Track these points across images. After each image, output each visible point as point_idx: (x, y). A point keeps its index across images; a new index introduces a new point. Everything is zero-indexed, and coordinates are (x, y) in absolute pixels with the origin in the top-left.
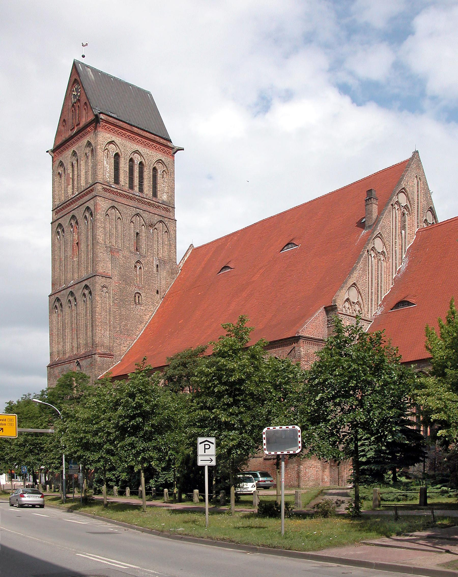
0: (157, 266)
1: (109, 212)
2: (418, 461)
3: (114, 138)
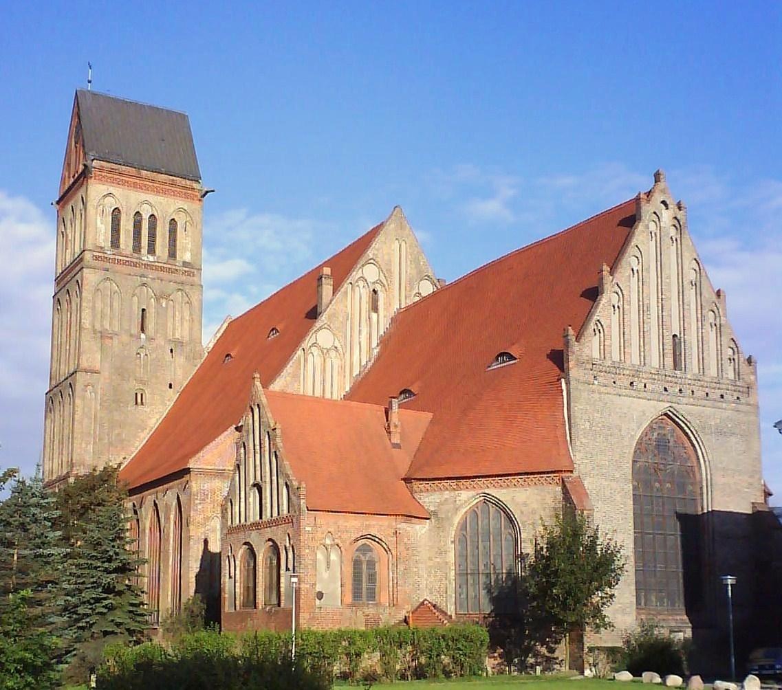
0: (172, 351)
1: (101, 286)
2: (139, 664)
3: (112, 190)
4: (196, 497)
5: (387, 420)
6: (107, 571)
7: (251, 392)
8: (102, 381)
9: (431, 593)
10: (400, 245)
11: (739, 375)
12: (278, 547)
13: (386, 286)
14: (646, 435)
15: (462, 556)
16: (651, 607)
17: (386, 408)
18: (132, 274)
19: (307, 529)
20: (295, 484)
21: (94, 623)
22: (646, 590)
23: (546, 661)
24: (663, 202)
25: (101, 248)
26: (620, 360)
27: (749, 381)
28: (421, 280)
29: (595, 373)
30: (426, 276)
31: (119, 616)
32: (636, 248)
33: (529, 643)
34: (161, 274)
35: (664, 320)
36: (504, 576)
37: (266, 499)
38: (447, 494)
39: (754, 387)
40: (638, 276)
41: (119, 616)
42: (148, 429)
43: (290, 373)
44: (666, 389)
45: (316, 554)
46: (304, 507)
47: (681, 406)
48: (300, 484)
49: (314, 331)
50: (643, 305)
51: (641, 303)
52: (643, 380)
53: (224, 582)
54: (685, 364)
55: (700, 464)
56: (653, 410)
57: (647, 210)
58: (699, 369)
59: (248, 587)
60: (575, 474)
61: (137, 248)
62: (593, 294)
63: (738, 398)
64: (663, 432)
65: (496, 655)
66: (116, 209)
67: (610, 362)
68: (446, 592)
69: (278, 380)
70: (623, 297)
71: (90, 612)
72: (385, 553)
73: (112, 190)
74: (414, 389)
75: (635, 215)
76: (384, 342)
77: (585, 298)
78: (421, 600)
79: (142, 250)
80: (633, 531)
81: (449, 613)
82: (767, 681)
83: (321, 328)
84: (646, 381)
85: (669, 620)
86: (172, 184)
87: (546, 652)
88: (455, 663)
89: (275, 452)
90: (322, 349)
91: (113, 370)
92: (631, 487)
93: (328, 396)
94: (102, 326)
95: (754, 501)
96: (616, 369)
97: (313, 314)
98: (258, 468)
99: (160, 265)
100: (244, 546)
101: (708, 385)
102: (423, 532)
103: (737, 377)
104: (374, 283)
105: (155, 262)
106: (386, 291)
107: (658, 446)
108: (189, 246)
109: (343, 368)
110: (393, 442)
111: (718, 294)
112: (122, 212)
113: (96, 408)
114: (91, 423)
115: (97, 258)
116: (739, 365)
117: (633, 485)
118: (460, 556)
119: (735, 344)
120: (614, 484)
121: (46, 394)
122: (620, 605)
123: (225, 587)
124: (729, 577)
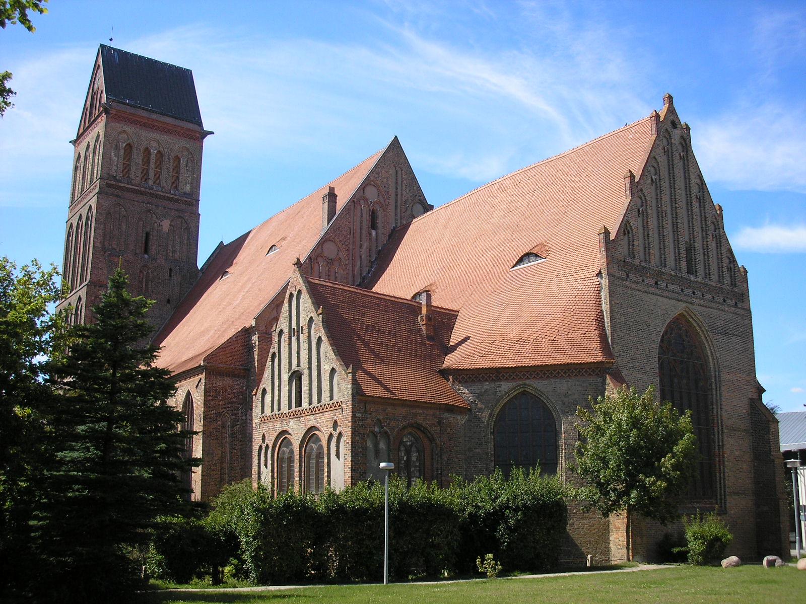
47: (695, 307)
67: (639, 261)
73: (125, 128)
95: (750, 397)
120: (645, 377)
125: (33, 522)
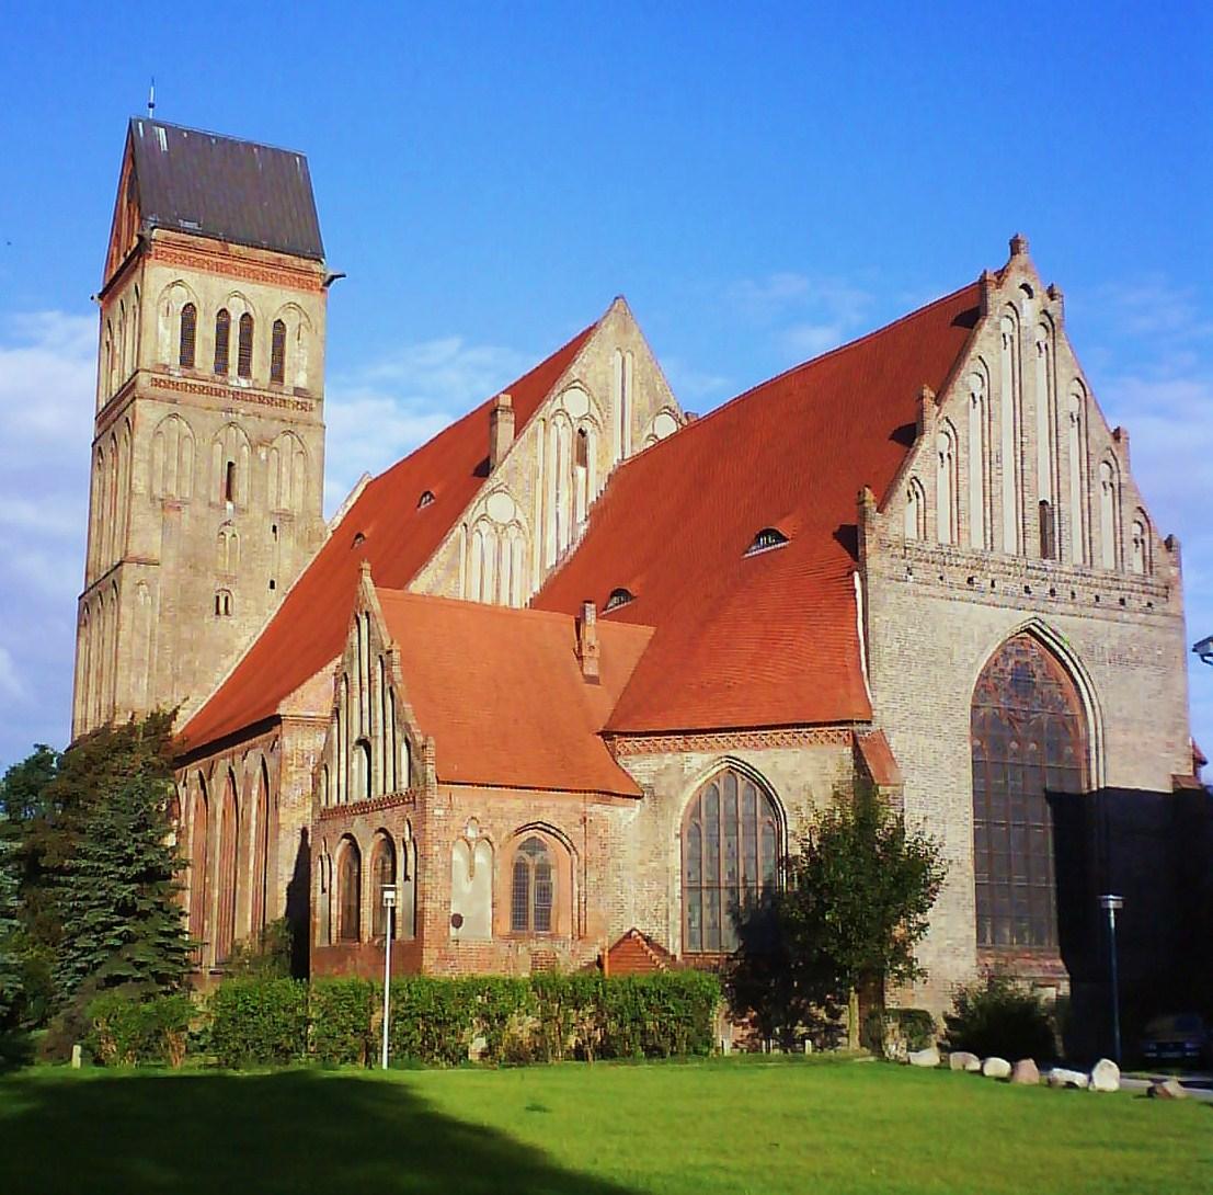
0: (274, 529)
1: (163, 428)
4: (290, 762)
5: (579, 639)
6: (123, 879)
7: (358, 592)
8: (163, 578)
9: (643, 919)
10: (624, 359)
11: (1151, 567)
12: (393, 842)
13: (600, 422)
14: (996, 665)
15: (693, 859)
16: (1002, 945)
17: (576, 619)
18: (214, 407)
19: (437, 812)
20: (420, 739)
21: (100, 963)
22: (993, 917)
23: (825, 1031)
24: (1025, 287)
25: (165, 366)
26: (952, 542)
27: (1169, 577)
28: (657, 415)
29: (909, 562)
30: (665, 408)
31: (141, 953)
32: (979, 361)
33: (798, 1003)
34: (259, 408)
35: (1025, 477)
36: (760, 892)
37: (376, 765)
38: (668, 758)
39: (1177, 587)
40: (983, 406)
41: (141, 953)
42: (236, 653)
43: (443, 563)
44: (1027, 590)
45: (451, 853)
46: (432, 778)
47: (1052, 617)
48: (426, 740)
49: (483, 495)
50: (990, 452)
51: (987, 449)
52: (990, 575)
53: (315, 898)
54: (1060, 549)
55: (1086, 713)
56: (1006, 623)
57: (996, 299)
58: (1084, 556)
59: (350, 906)
60: (875, 727)
61: (221, 366)
62: (908, 435)
63: (1150, 605)
64: (1023, 659)
65: (746, 1020)
66: (189, 304)
67: (934, 545)
68: (667, 917)
69: (422, 574)
70: (957, 440)
71: (95, 944)
72: (567, 853)
73: (183, 275)
74: (632, 589)
75: (978, 308)
76: (597, 513)
77: (897, 441)
78: (627, 930)
79: (230, 370)
80: (972, 820)
81: (671, 952)
82: (1169, 1070)
83: (493, 491)
84: (994, 576)
85: (1031, 966)
86: (278, 264)
87: (825, 1016)
88: (663, 1033)
89: (391, 689)
90: (495, 525)
91: (181, 559)
92: (969, 749)
93: (504, 601)
94: (164, 489)
95: (1174, 773)
96: (944, 557)
97: (484, 470)
98: (366, 715)
99: (257, 393)
100: (344, 840)
101: (1099, 583)
102: (633, 816)
103: (1147, 570)
104: (580, 419)
105: (249, 388)
106: (601, 432)
107: (1015, 682)
108: (305, 363)
109: (529, 555)
110: (586, 673)
111: (1117, 435)
112: (198, 310)
113: (152, 620)
114: (144, 644)
115: (156, 383)
116: (1151, 551)
117: (973, 747)
118: (690, 858)
119: (1145, 516)
120: (939, 744)
121: (80, 598)
122: (949, 942)
123: (315, 907)
124: (1111, 897)
125: (1057, 1043)
